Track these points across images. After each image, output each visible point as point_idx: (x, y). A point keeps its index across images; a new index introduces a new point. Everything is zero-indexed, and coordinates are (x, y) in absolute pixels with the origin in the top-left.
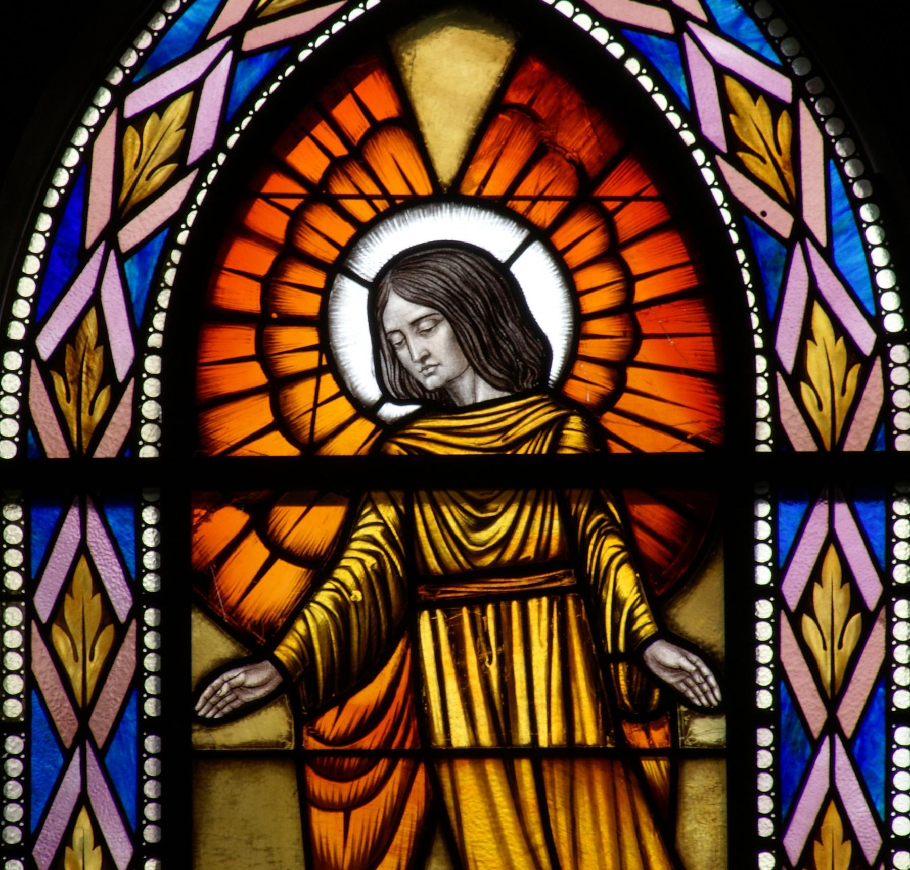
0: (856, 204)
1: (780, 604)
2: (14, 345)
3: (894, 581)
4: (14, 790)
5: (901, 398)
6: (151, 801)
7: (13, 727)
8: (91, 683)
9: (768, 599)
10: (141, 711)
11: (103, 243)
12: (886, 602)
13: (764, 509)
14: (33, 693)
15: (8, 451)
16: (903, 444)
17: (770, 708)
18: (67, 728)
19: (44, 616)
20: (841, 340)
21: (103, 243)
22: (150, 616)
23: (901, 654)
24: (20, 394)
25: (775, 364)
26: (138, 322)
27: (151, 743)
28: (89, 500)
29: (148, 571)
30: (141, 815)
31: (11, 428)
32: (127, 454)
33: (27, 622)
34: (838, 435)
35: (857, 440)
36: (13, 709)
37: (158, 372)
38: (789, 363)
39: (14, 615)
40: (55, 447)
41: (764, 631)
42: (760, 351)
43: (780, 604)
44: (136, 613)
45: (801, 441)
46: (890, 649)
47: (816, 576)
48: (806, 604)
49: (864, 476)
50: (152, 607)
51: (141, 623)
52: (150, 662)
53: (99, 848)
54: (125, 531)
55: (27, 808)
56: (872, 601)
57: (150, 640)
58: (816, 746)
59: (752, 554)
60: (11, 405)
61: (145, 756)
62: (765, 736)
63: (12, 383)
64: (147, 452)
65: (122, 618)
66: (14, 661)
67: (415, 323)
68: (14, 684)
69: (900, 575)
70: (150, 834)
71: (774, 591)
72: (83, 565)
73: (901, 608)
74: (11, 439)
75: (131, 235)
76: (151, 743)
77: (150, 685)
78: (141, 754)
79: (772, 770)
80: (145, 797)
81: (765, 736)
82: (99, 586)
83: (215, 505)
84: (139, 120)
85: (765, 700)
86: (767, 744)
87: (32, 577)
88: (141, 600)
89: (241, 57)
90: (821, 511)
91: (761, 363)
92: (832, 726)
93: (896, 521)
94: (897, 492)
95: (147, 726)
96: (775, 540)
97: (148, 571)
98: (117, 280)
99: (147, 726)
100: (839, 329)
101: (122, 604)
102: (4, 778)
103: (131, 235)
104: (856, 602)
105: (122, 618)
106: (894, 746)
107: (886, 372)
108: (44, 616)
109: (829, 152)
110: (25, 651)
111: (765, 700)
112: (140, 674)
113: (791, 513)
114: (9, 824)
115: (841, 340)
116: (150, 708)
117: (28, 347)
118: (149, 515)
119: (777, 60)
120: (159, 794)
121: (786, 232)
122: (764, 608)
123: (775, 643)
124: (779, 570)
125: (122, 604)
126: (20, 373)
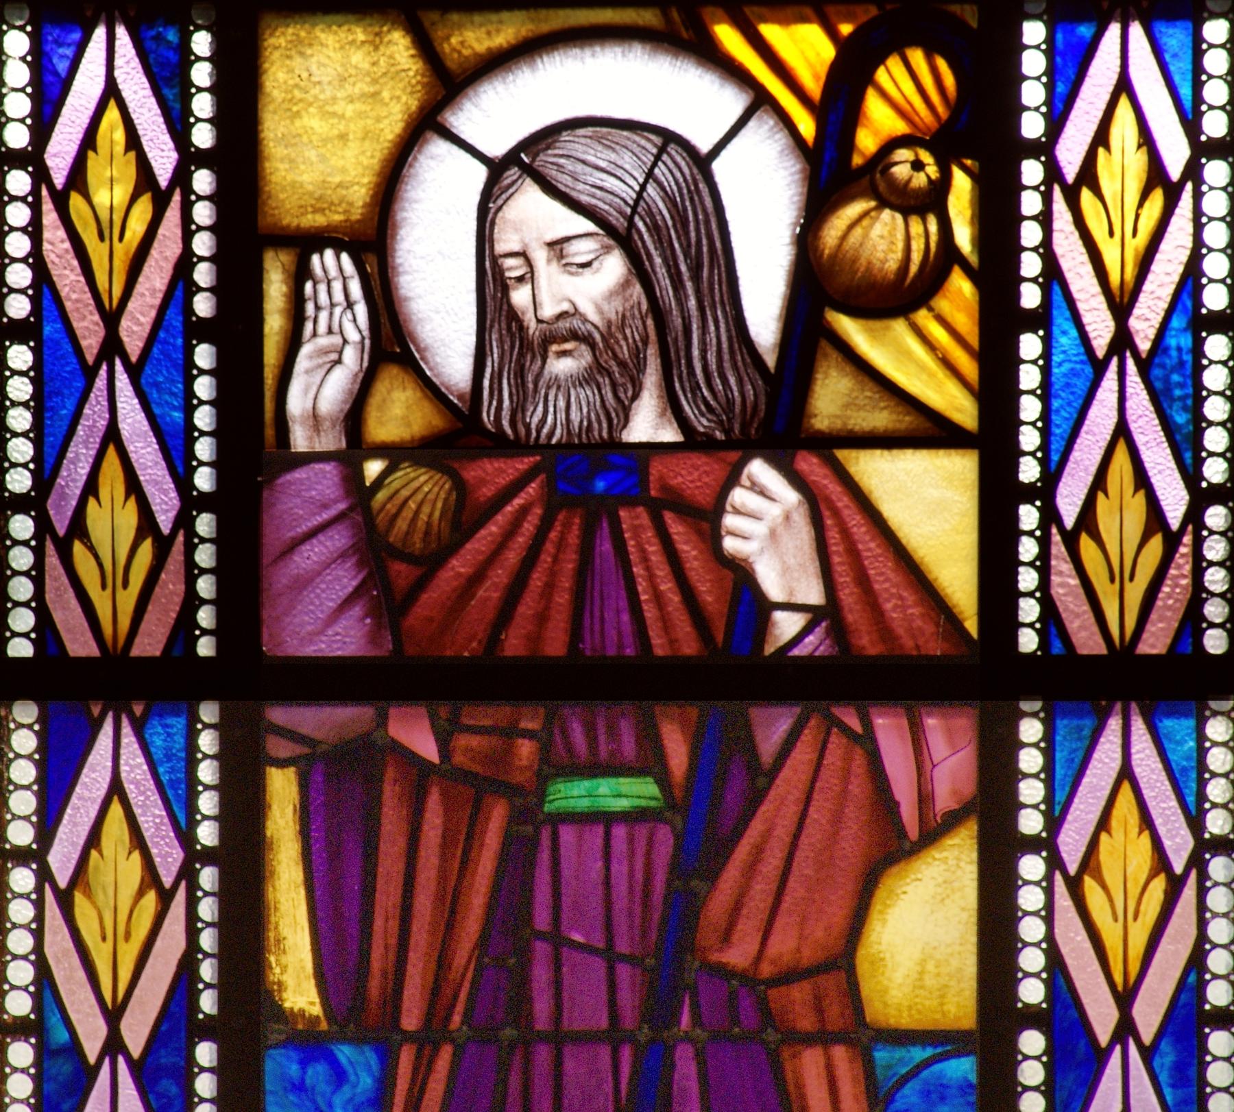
4: (19, 419)
8: (125, 623)
9: (1038, 159)
12: (1197, 862)
14: (47, 886)
17: (1036, 651)
19: (59, 179)
22: (205, 524)
27: (204, 355)
29: (204, 602)
32: (176, 653)
33: (39, 535)
36: (18, 307)
37: (214, 535)
39: (22, 879)
41: (1031, 203)
46: (1202, 924)
47: (1102, 137)
48: (1088, 175)
50: (207, 511)
51: (191, 533)
52: (207, 940)
55: (38, 444)
61: (196, 541)
63: (18, 215)
66: (21, 589)
67: (557, 247)
68: (19, 276)
69: (1217, 824)
70: (204, 480)
71: (1047, 844)
72: (116, 809)
73: (1218, 867)
76: (204, 355)
78: (189, 371)
79: (1043, 1088)
87: (44, 120)
94: (1210, 709)
95: (199, 330)
97: (204, 602)
99: (199, 330)
102: (3, 120)
104: (1156, 173)
105: (166, 529)
107: (1202, 893)
108: (59, 179)
112: (186, 262)
114: (12, 290)
116: (203, 306)
118: (201, 42)
119: (1057, 289)
120: (214, 251)
123: (1048, 914)
124: (1054, 822)
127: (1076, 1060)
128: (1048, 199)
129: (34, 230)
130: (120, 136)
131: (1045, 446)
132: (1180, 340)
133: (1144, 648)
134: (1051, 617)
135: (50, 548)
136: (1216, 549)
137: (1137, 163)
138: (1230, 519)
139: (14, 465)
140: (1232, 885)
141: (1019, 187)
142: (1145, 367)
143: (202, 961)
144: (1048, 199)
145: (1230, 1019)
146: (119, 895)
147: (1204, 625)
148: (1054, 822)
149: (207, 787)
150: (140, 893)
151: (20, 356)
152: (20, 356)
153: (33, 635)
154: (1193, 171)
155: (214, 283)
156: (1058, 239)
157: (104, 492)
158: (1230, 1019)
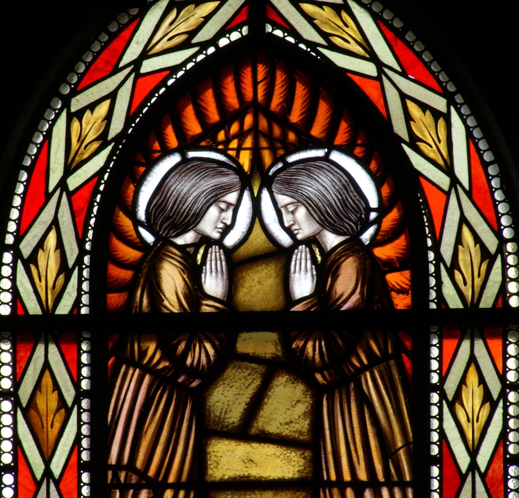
0: (485, 165)
1: (443, 396)
2: (8, 248)
3: (508, 380)
5: (512, 287)
6: (85, 365)
7: (7, 469)
9: (436, 466)
10: (80, 458)
11: (59, 189)
13: (435, 341)
15: (6, 311)
16: (514, 302)
18: (39, 469)
20: (478, 246)
21: (59, 189)
22: (85, 403)
23: (512, 423)
24: (11, 277)
25: (439, 258)
26: (81, 237)
27: (85, 477)
28: (50, 336)
30: (79, 374)
31: (7, 297)
33: (14, 409)
34: (475, 300)
35: (487, 301)
36: (7, 459)
38: (448, 261)
40: (33, 308)
42: (431, 249)
43: (443, 396)
44: (77, 401)
45: (454, 302)
49: (491, 322)
51: (80, 407)
53: (56, 392)
54: (71, 356)
56: (495, 395)
57: (85, 417)
58: (463, 478)
59: (429, 424)
60: (6, 284)
62: (435, 471)
63: (6, 271)
64: (84, 311)
65: (70, 404)
68: (7, 446)
70: (85, 385)
71: (440, 388)
74: (7, 304)
75: (74, 182)
77: (85, 443)
78: (79, 484)
80: (82, 363)
81: (435, 471)
82: (56, 387)
83: (121, 472)
84: (80, 114)
85: (435, 450)
86: (435, 356)
88: (80, 394)
89: (139, 76)
90: (466, 345)
91: (431, 256)
92: (473, 466)
93: (509, 268)
95: (83, 467)
96: (440, 359)
98: (67, 207)
99: (83, 467)
100: (477, 240)
101: (69, 396)
103: (74, 182)
104: (487, 397)
105: (70, 404)
106: (507, 369)
107: (506, 408)
109: (469, 136)
110: (13, 351)
111: (435, 450)
113: (450, 344)
115: (478, 246)
116: (85, 456)
117: (15, 249)
121: (446, 187)
122: (435, 398)
123: (441, 419)
125: (69, 396)
126: (11, 265)
127: (454, 480)
128: (441, 408)
129: (15, 427)
130: (50, 383)
131: (440, 368)
132: (498, 465)
133: (482, 305)
134: (441, 299)
135: (19, 413)
136: (511, 260)
137: (479, 392)
138: (518, 273)
139: (6, 486)
140: (518, 404)
141: (430, 404)
142: (483, 476)
143: (83, 438)
144: (441, 408)
145: (518, 460)
146: (49, 262)
147: (508, 266)
148: (443, 379)
149: (85, 436)
150: (58, 410)
151: (8, 479)
152: (8, 479)
153: (12, 440)
154: (503, 395)
155: (90, 375)
156: (445, 426)
157: (44, 389)
158: (518, 460)
